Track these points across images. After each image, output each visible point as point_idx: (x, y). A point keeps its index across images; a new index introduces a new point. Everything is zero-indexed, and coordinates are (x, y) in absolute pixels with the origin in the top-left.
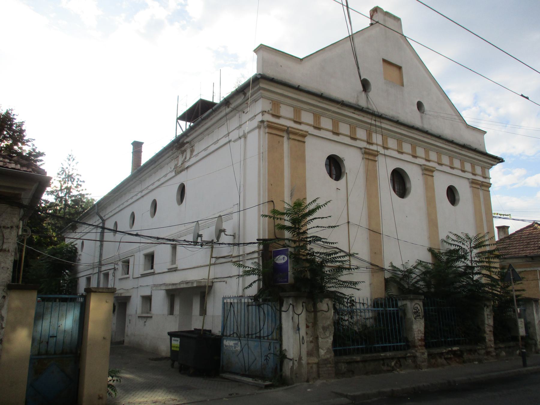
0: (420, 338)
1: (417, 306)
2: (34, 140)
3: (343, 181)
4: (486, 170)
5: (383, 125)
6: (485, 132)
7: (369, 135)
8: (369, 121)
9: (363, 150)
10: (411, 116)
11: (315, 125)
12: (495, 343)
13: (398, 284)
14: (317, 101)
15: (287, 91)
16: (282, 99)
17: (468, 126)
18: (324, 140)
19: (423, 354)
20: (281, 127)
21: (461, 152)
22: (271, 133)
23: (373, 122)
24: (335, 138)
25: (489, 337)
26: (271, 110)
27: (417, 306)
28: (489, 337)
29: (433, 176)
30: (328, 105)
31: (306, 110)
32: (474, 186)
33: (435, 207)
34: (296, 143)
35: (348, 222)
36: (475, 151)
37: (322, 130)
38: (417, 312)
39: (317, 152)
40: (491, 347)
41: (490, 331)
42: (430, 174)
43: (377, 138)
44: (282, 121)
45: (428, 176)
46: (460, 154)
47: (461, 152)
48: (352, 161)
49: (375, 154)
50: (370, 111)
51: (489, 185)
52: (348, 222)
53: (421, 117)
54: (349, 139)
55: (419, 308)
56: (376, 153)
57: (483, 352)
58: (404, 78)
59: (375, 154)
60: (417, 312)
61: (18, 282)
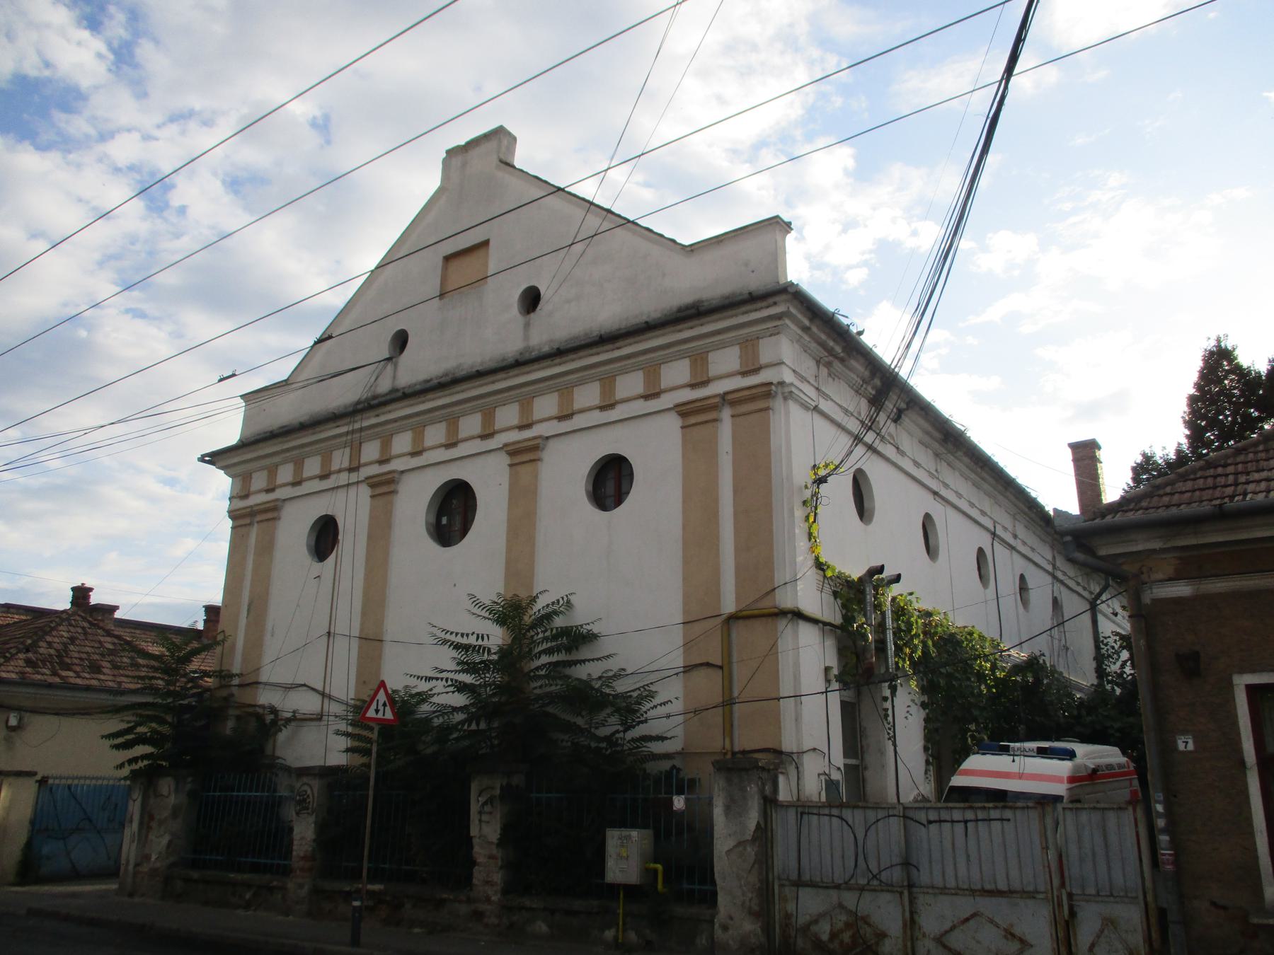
0: (302, 854)
1: (306, 788)
5: (366, 423)
8: (344, 429)
12: (505, 892)
13: (398, 737)
16: (276, 459)
17: (693, 249)
18: (650, 418)
19: (301, 886)
21: (617, 354)
22: (241, 526)
23: (357, 426)
25: (488, 871)
27: (306, 788)
28: (488, 871)
30: (528, 373)
33: (531, 540)
38: (304, 800)
40: (488, 900)
41: (491, 857)
47: (617, 354)
52: (329, 633)
53: (527, 326)
54: (555, 422)
55: (309, 792)
56: (764, 389)
57: (464, 909)
60: (304, 800)
61: (369, 741)
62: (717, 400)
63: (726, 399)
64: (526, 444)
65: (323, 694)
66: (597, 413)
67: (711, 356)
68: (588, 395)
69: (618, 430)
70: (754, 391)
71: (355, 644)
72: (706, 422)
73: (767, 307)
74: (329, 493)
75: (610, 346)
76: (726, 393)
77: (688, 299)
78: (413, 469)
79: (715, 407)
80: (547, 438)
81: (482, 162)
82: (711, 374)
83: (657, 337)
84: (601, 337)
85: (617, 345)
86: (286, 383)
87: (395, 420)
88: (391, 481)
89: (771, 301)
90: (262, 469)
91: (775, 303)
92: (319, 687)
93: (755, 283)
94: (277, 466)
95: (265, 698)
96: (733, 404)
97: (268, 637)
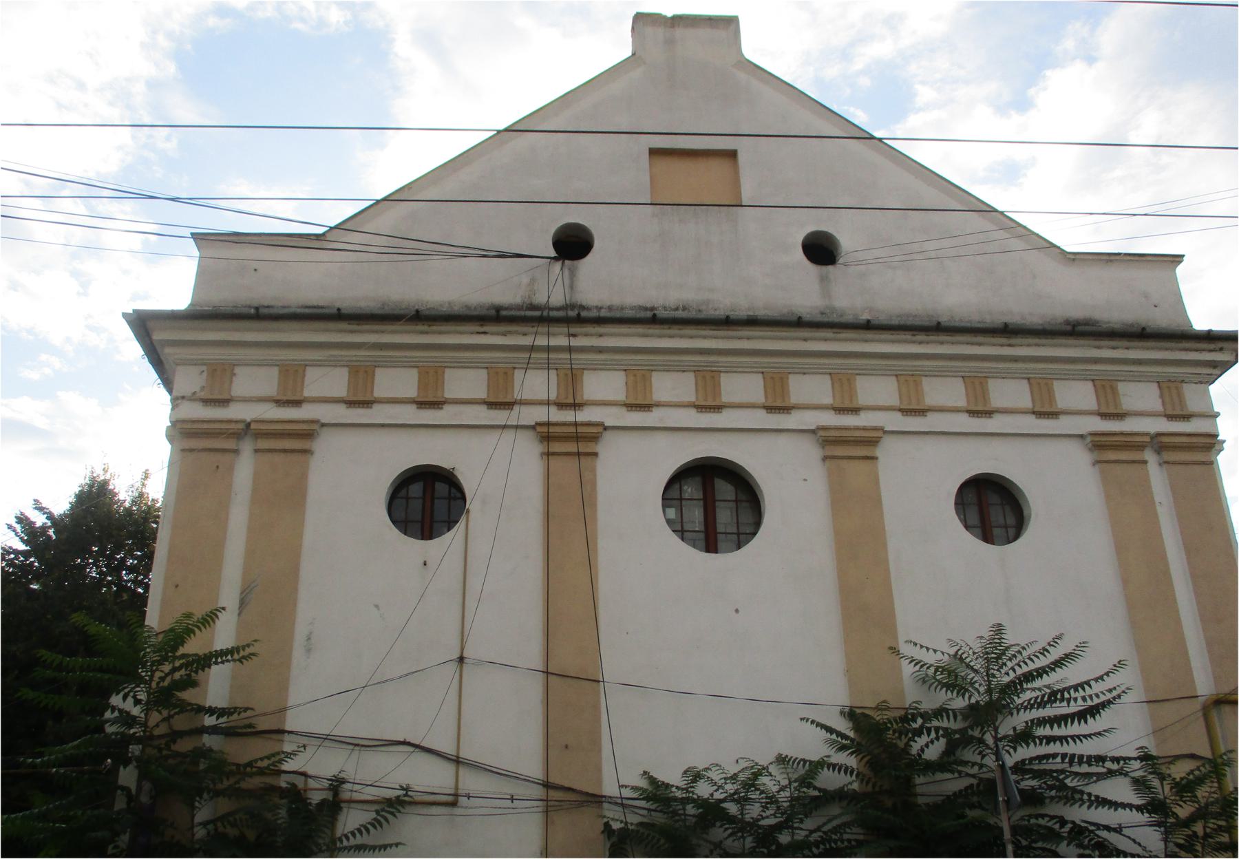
2: (1059, 637)
3: (450, 540)
4: (1189, 391)
6: (1177, 259)
7: (572, 379)
8: (527, 341)
9: (1089, 439)
10: (803, 289)
11: (1104, 410)
14: (341, 331)
15: (237, 330)
20: (205, 426)
22: (191, 450)
23: (541, 341)
24: (429, 416)
26: (203, 388)
29: (874, 458)
31: (1065, 377)
32: (1112, 455)
34: (278, 458)
35: (461, 659)
36: (1141, 335)
37: (1061, 417)
39: (631, 477)
42: (1199, 457)
43: (604, 386)
44: (237, 412)
45: (844, 463)
46: (1015, 359)
48: (500, 473)
49: (869, 440)
50: (326, 311)
51: (1210, 443)
52: (461, 659)
53: (824, 279)
58: (743, 181)
59: (869, 440)
62: (1147, 439)
63: (246, 430)
64: (857, 434)
65: (457, 761)
66: (412, 408)
67: (379, 373)
68: (397, 382)
69: (997, 446)
70: (1195, 440)
71: (534, 689)
72: (1133, 462)
73: (1211, 351)
74: (498, 433)
75: (425, 328)
76: (1159, 435)
77: (1077, 314)
78: (383, 426)
79: (1141, 447)
80: (323, 425)
81: (691, 43)
82: (517, 396)
83: (1066, 346)
84: (1006, 325)
85: (1013, 341)
86: (318, 237)
87: (600, 350)
88: (309, 435)
89: (1220, 345)
90: (194, 363)
91: (1221, 349)
92: (449, 749)
93: (1160, 319)
94: (305, 365)
95: (318, 765)
96: (259, 435)
97: (298, 654)
